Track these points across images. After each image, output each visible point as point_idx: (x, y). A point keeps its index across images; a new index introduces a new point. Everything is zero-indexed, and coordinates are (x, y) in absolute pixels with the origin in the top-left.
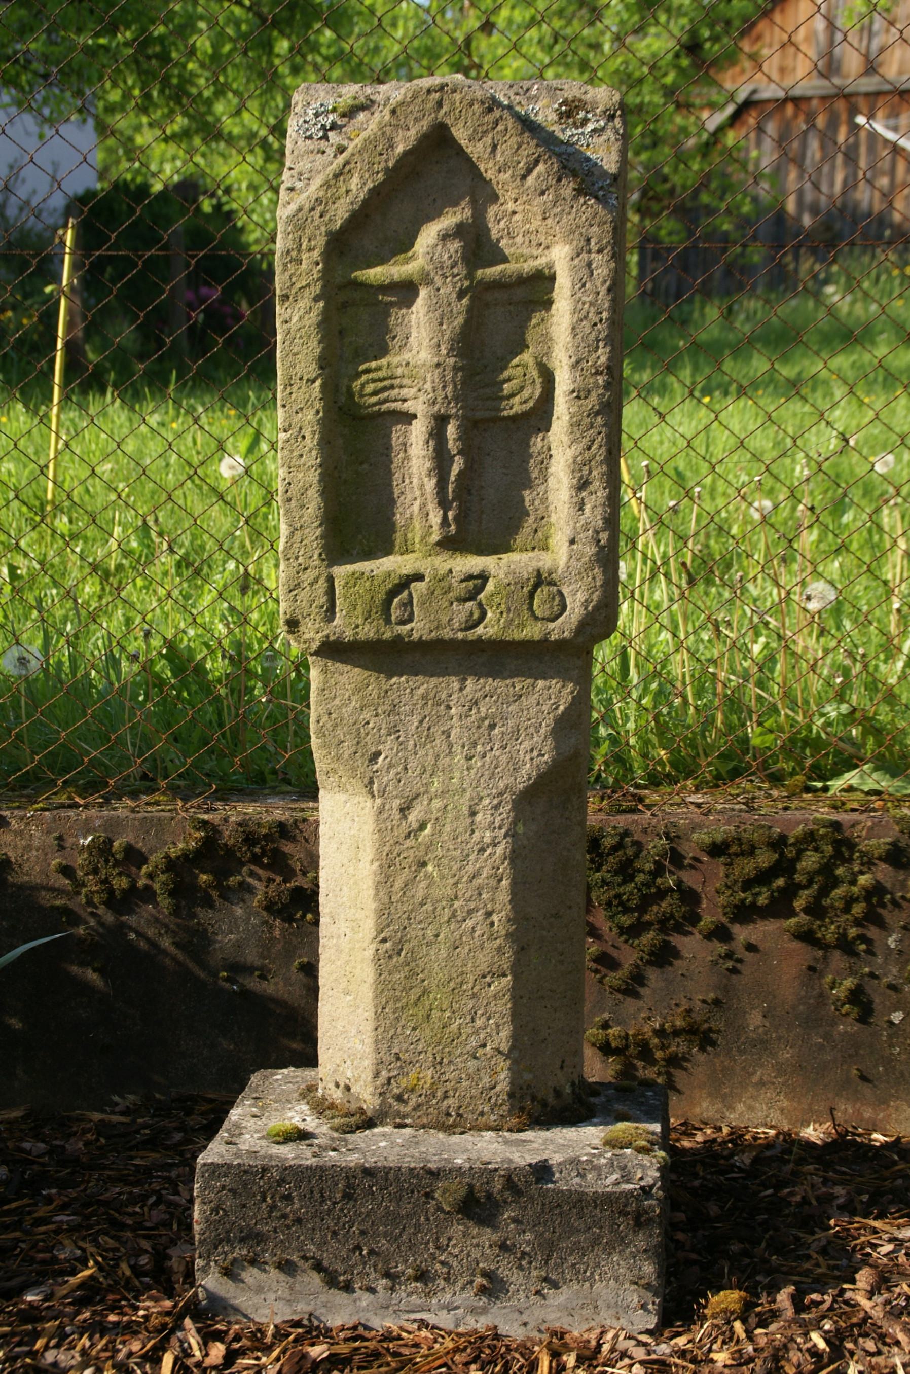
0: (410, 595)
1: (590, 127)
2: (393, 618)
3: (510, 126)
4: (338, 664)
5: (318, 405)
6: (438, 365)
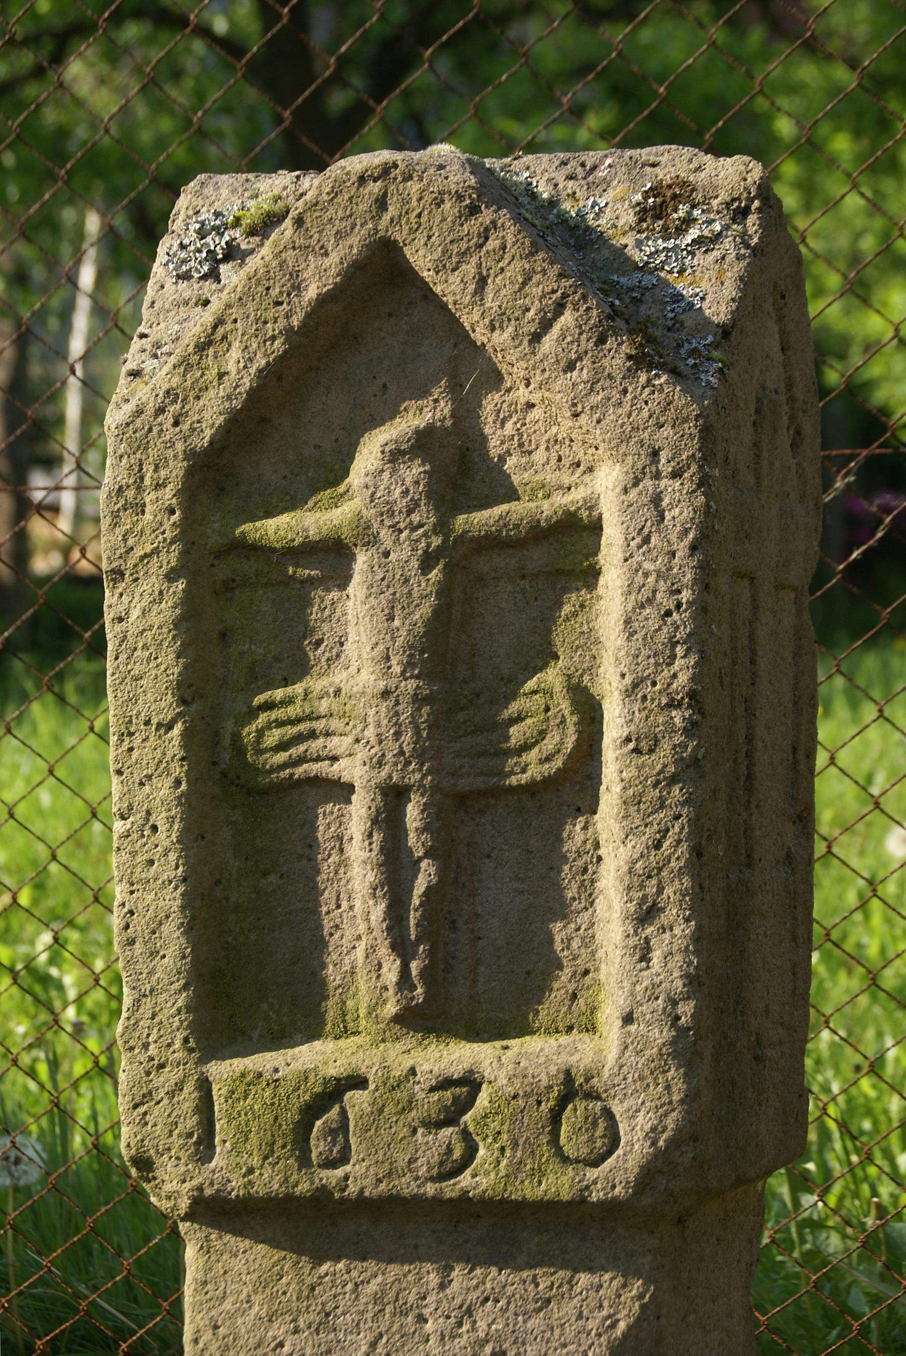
0: (343, 1113)
1: (693, 233)
2: (314, 1156)
3: (510, 239)
4: (228, 1237)
5: (177, 770)
6: (386, 694)
